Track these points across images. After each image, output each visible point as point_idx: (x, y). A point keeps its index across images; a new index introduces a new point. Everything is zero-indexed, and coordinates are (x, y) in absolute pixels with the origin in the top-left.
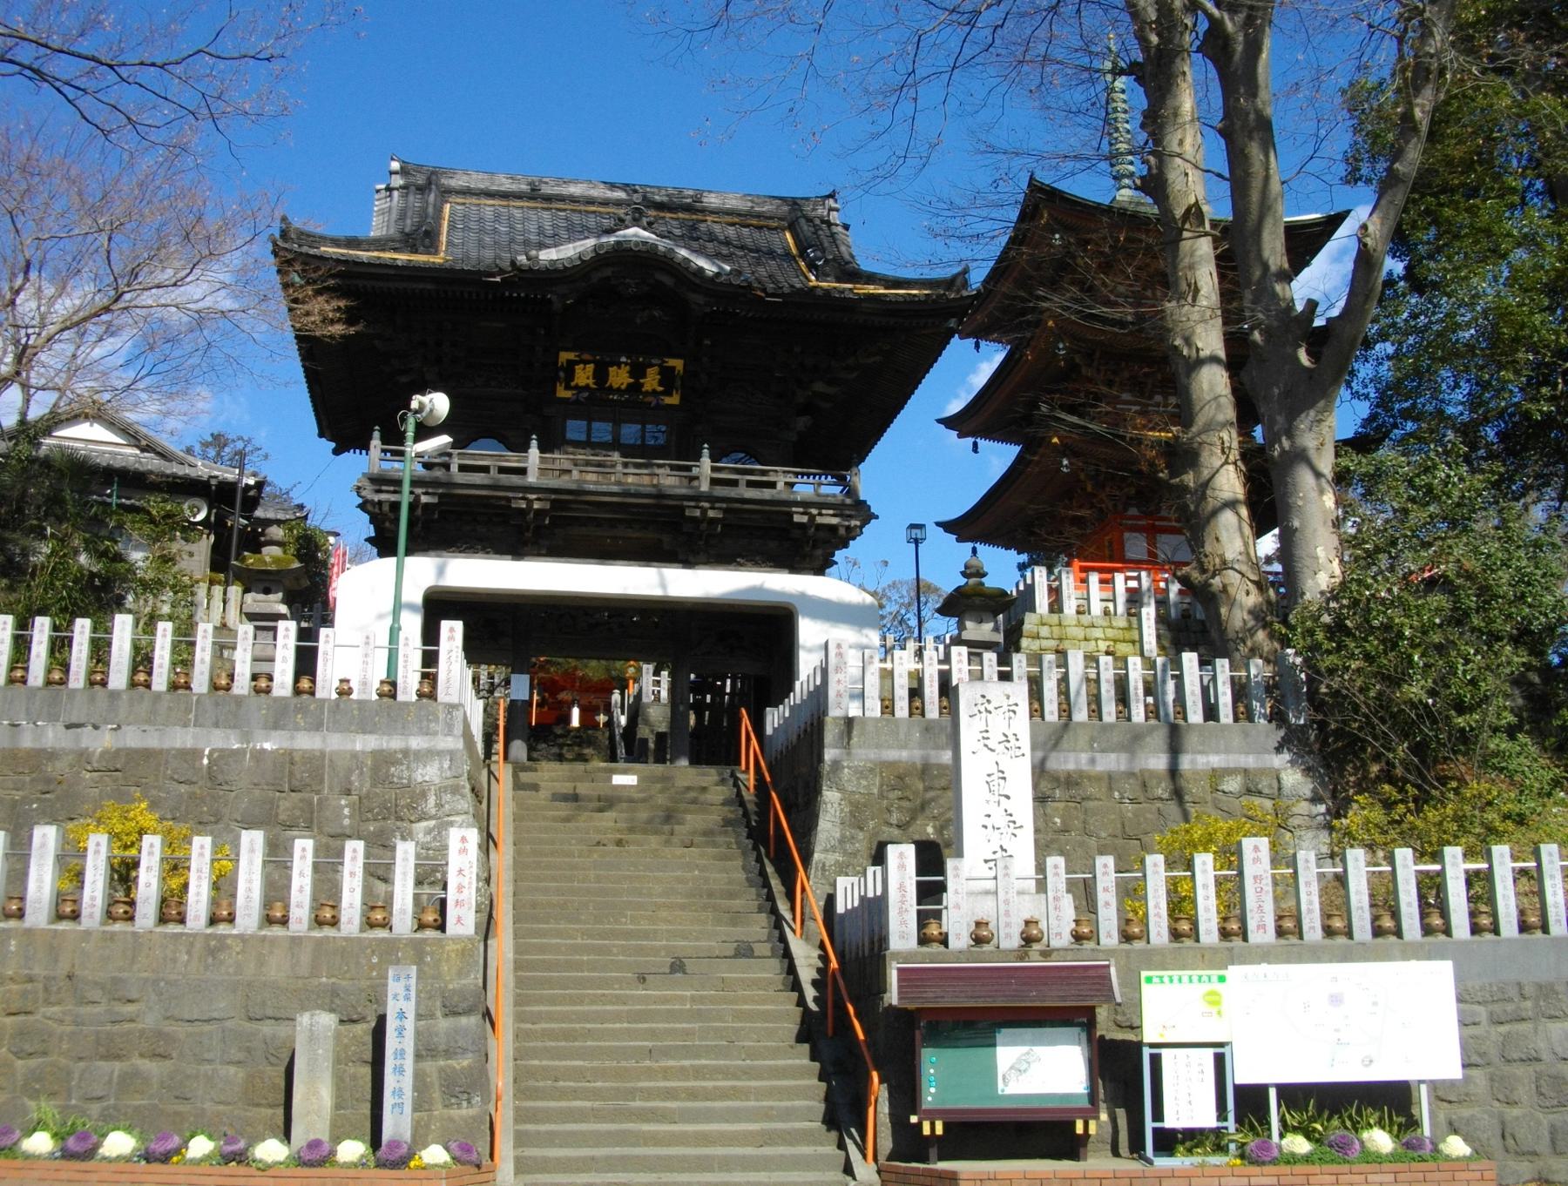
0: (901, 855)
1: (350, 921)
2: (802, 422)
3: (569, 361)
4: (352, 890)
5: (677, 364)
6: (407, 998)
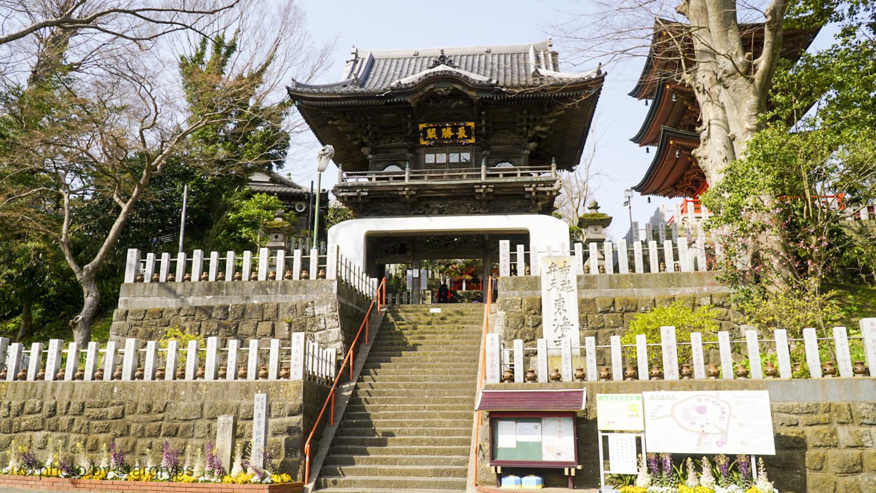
0: (298, 337)
2: (532, 145)
5: (472, 124)
6: (262, 408)
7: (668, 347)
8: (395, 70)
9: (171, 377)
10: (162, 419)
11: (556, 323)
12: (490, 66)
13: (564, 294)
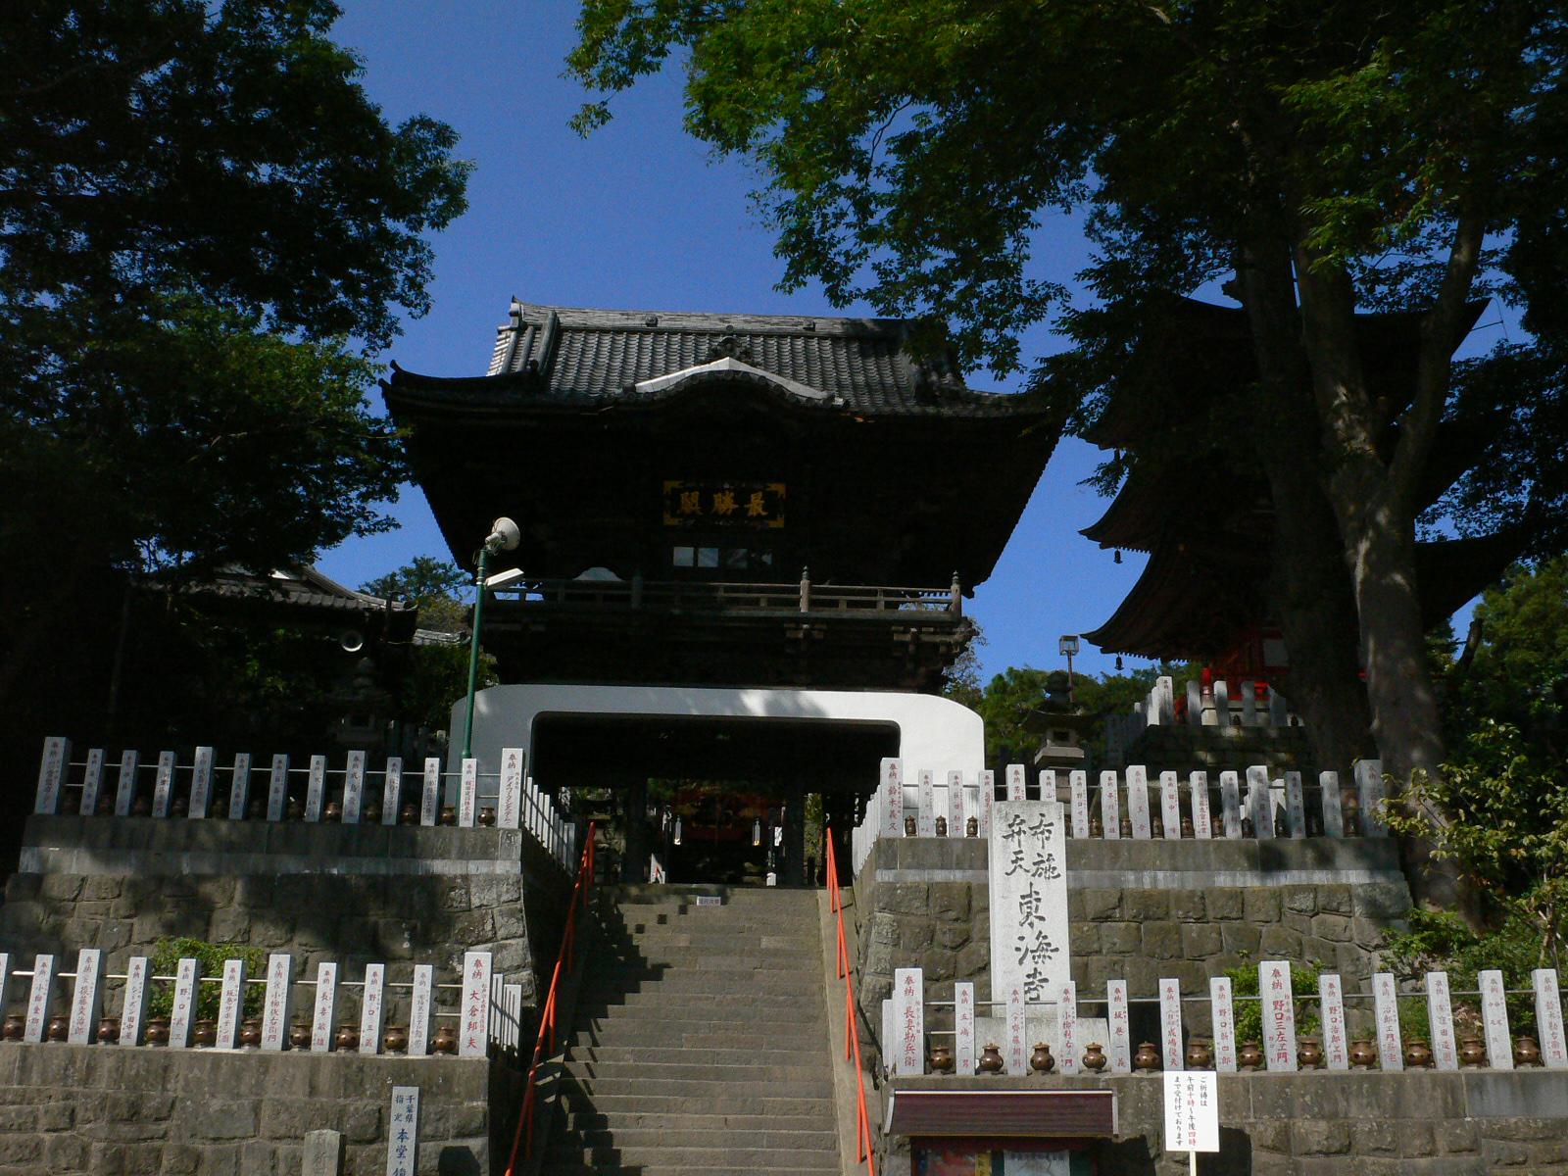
1: (79, 1031)
3: (673, 489)
4: (372, 1013)
5: (780, 488)
6: (409, 1118)
7: (1275, 1003)
8: (611, 358)
9: (183, 1042)
10: (164, 1137)
11: (1022, 945)
12: (818, 366)
13: (1040, 884)
